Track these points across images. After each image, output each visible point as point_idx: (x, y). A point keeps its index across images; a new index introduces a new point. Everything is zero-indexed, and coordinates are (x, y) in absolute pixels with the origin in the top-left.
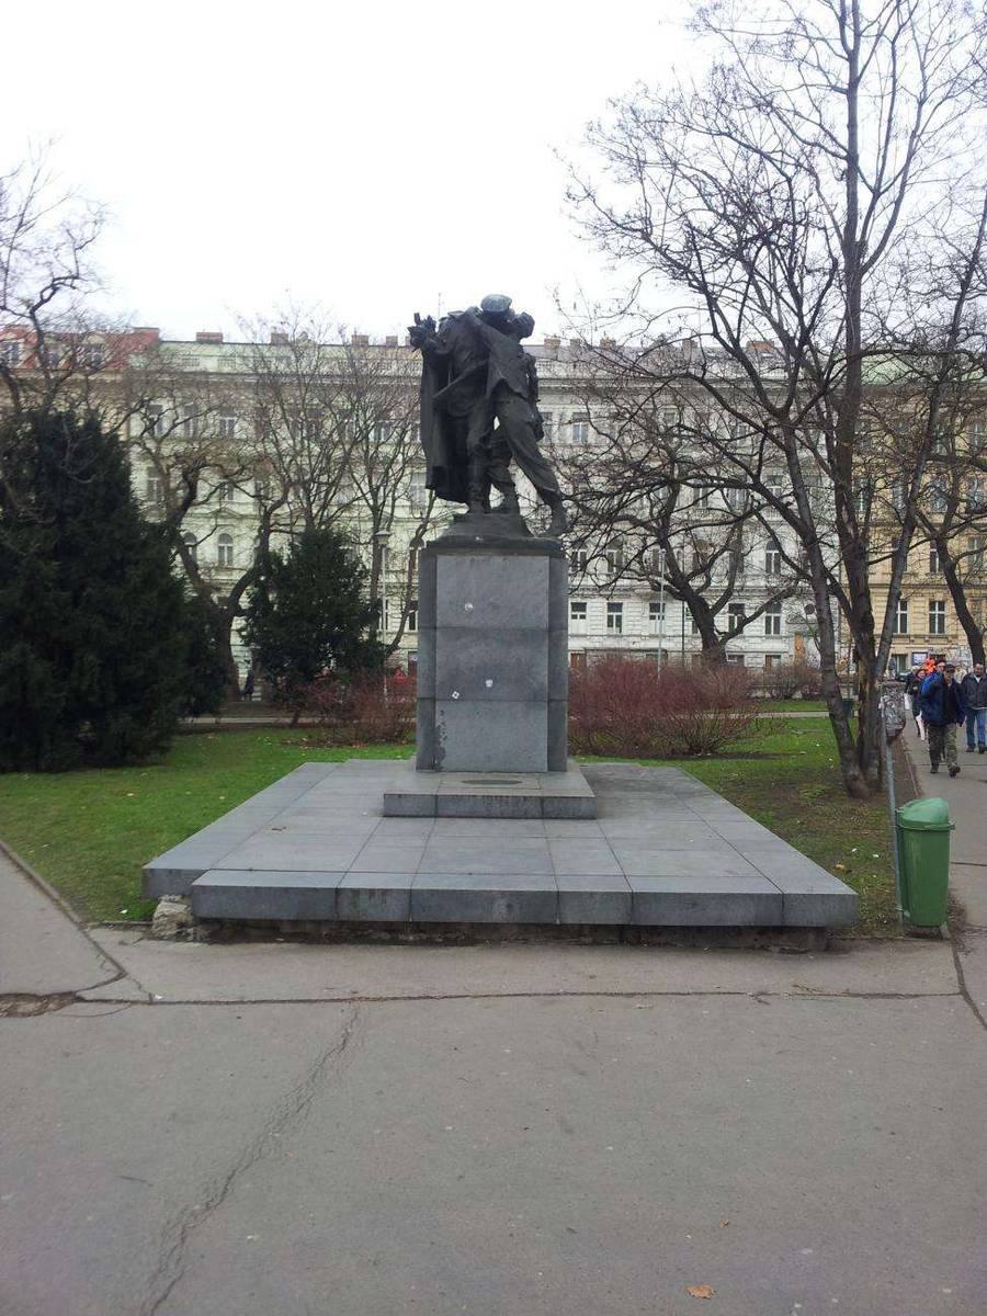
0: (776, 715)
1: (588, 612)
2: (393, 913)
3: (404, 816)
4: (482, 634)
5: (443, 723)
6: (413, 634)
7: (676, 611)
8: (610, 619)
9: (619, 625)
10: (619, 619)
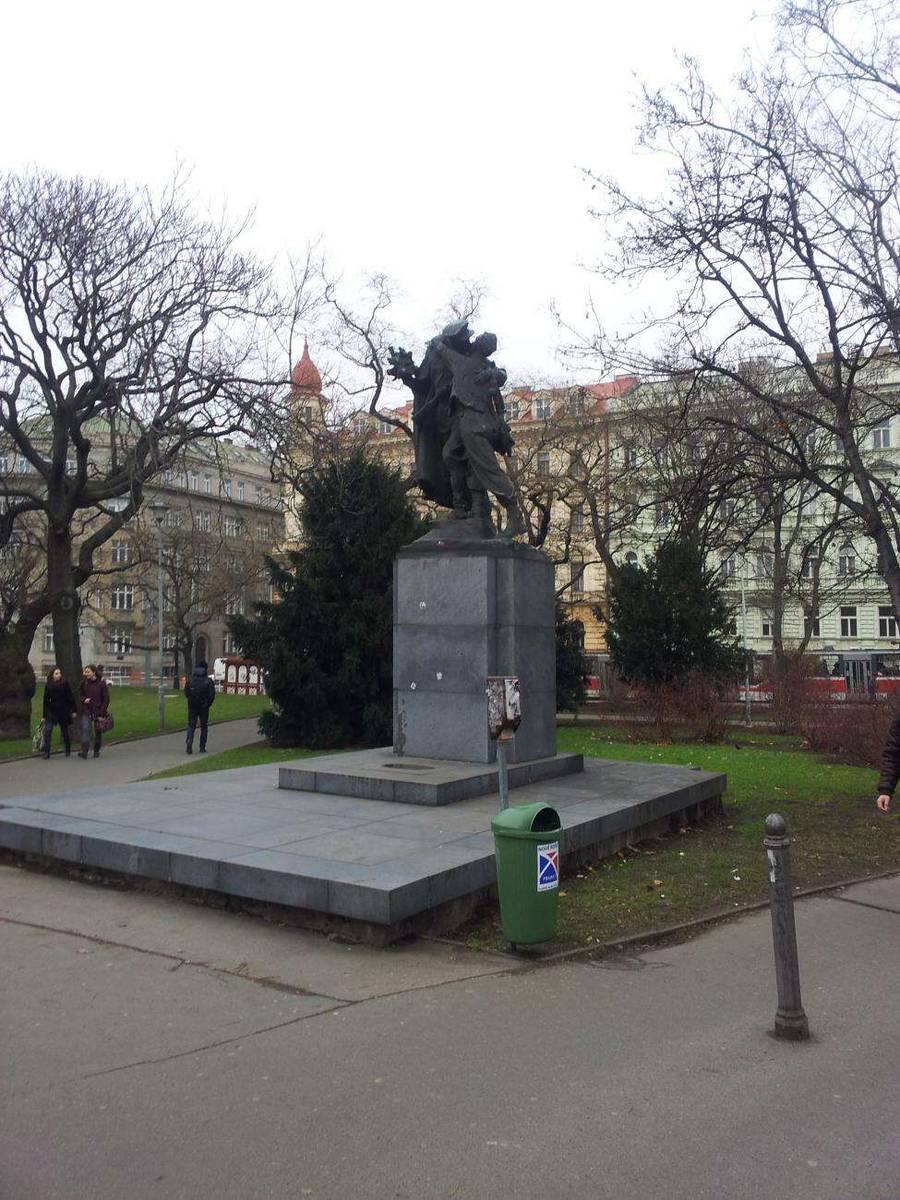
2: (70, 854)
3: (293, 789)
4: (434, 630)
6: (766, 639)
10: (854, 622)
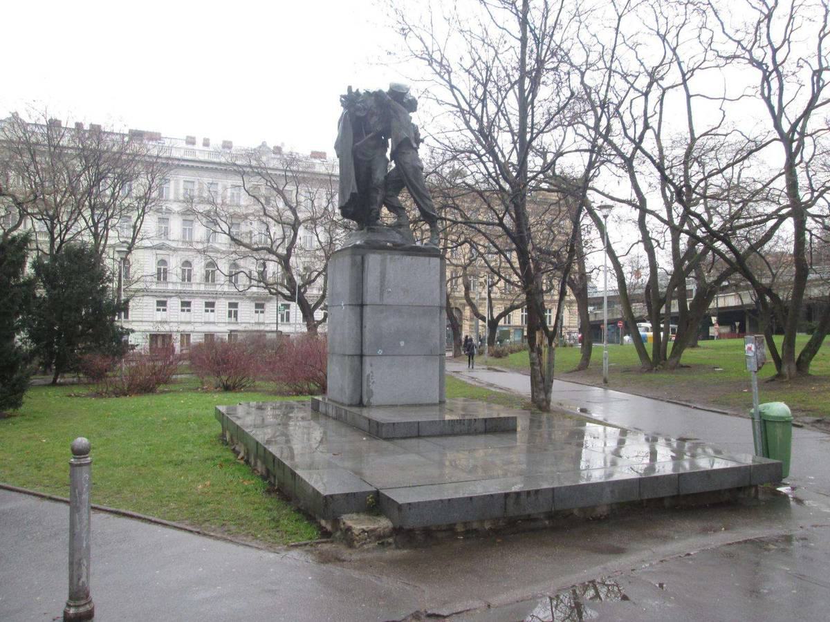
0: (732, 353)
1: (192, 307)
5: (372, 372)
7: (295, 310)
8: (230, 312)
9: (236, 316)
10: (236, 313)
